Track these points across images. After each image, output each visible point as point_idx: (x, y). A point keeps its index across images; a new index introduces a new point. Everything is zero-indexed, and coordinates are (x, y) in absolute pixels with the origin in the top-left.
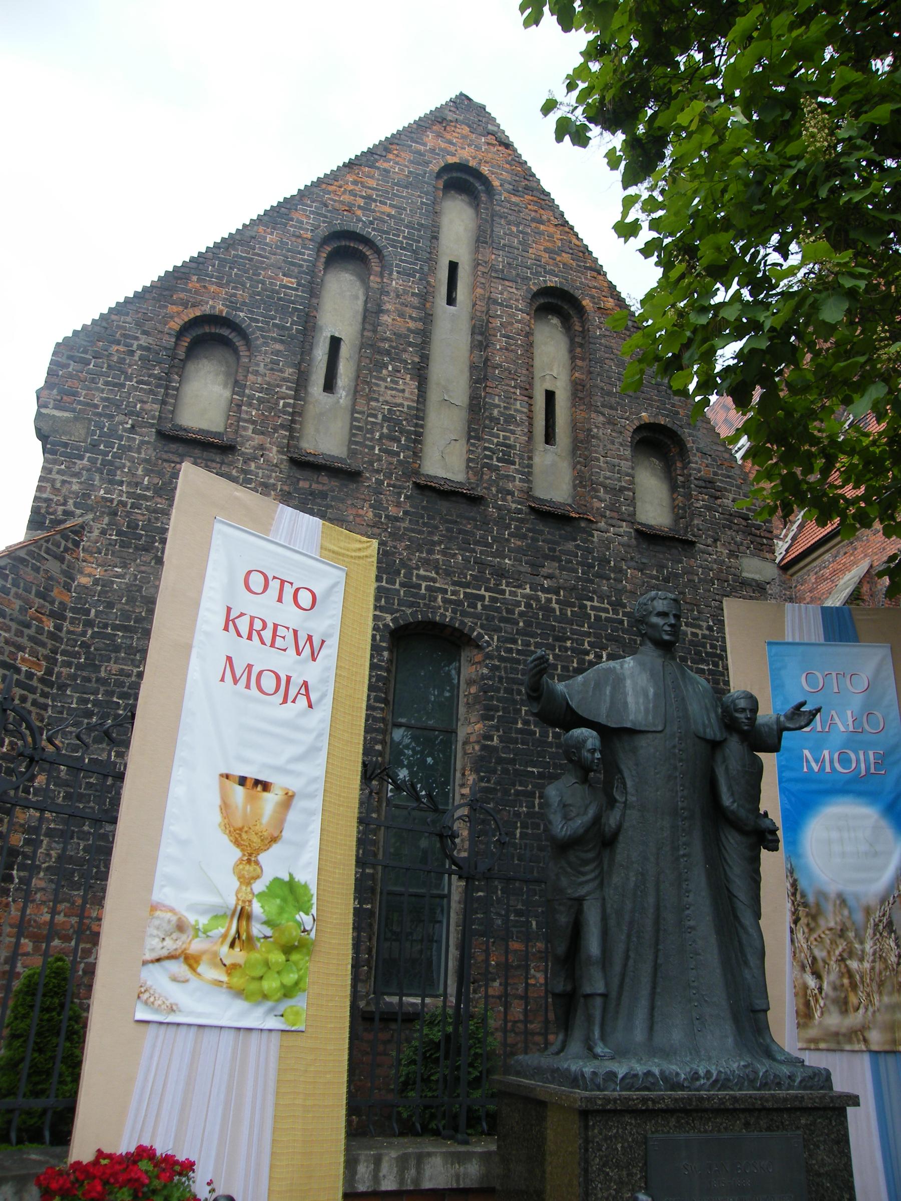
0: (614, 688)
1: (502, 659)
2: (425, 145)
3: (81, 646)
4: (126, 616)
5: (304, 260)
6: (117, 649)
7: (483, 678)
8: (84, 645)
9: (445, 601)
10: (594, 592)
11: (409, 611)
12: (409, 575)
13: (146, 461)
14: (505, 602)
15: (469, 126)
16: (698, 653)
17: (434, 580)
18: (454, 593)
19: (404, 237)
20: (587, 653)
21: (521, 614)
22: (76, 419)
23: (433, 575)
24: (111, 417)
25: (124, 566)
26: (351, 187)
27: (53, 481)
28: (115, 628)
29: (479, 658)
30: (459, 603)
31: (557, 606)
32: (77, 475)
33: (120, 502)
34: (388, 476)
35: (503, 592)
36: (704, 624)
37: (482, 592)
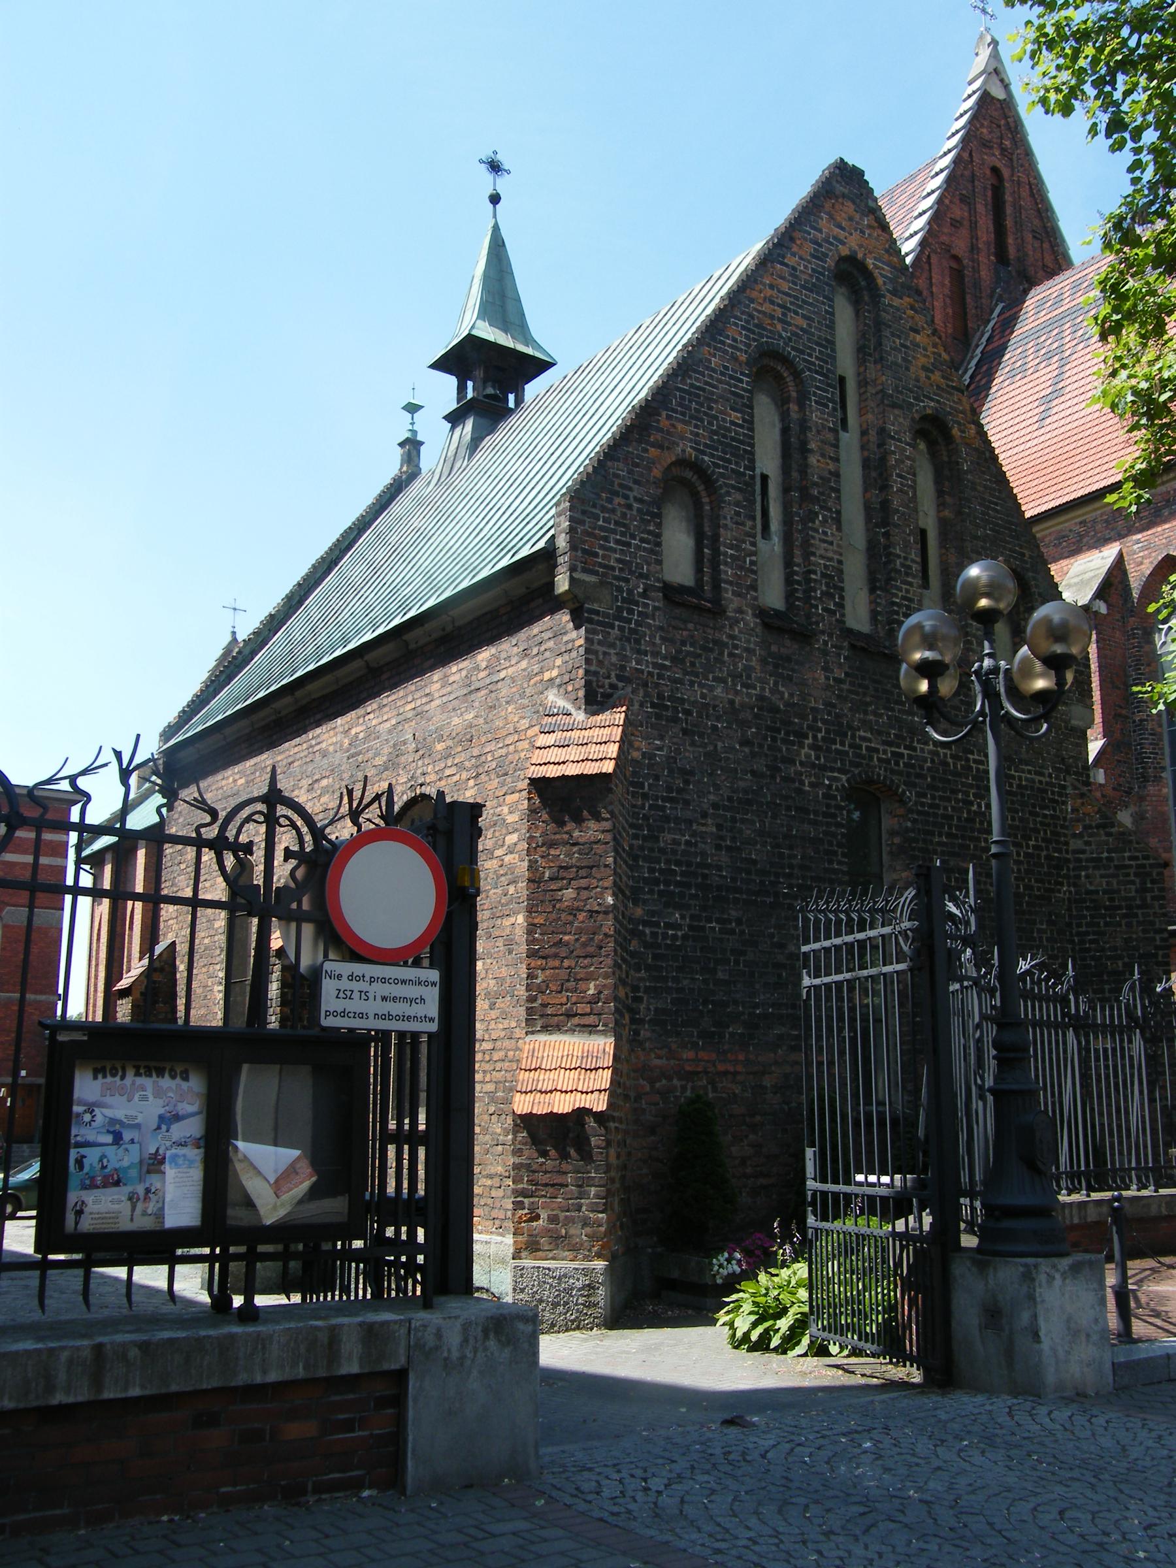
0: (709, 610)
1: (919, 813)
2: (820, 231)
3: (643, 819)
4: (669, 789)
5: (743, 389)
6: (667, 819)
7: (907, 830)
8: (646, 818)
9: (879, 759)
10: (974, 746)
11: (857, 772)
12: (853, 736)
13: (661, 628)
14: (917, 758)
15: (854, 202)
16: (1043, 799)
17: (870, 740)
18: (885, 752)
19: (817, 358)
20: (972, 803)
21: (929, 769)
22: (602, 583)
23: (869, 735)
24: (627, 581)
25: (661, 738)
26: (769, 292)
27: (596, 653)
28: (664, 799)
29: (900, 811)
30: (888, 761)
31: (950, 760)
32: (613, 645)
33: (649, 673)
34: (830, 635)
35: (915, 749)
36: (1046, 772)
37: (902, 750)
